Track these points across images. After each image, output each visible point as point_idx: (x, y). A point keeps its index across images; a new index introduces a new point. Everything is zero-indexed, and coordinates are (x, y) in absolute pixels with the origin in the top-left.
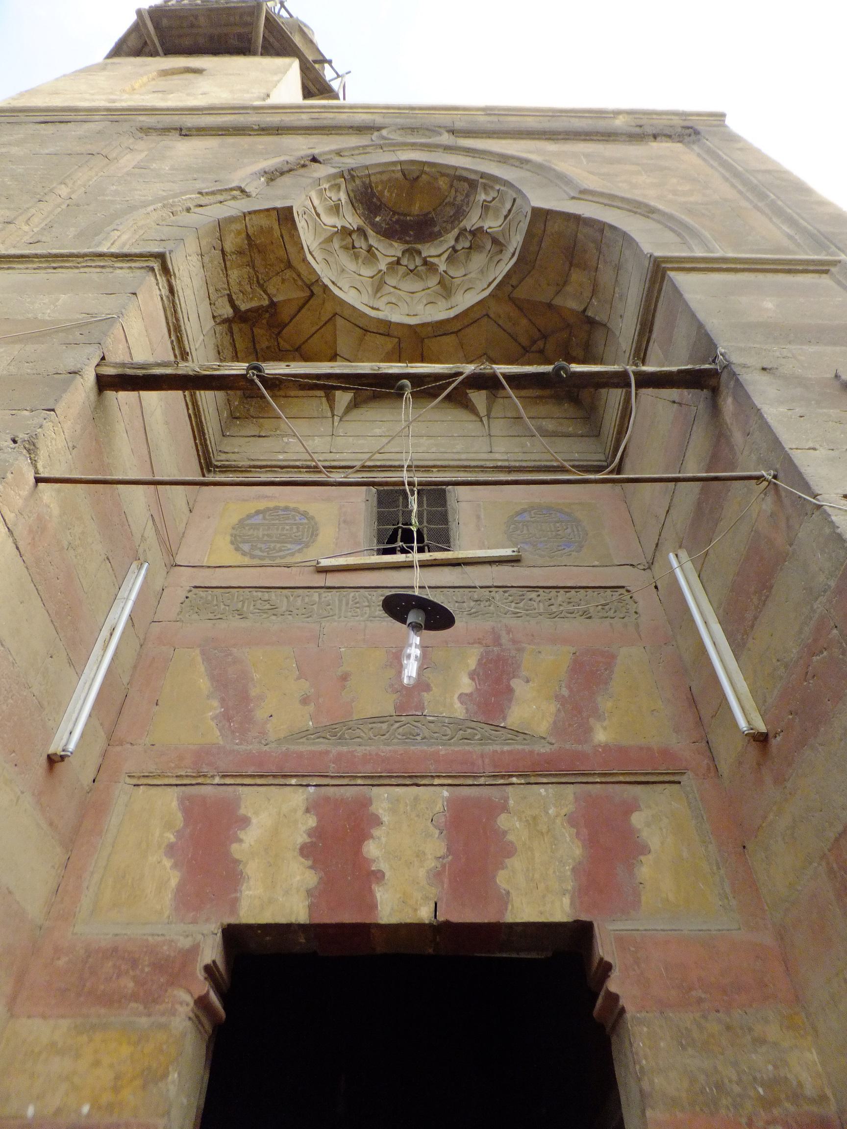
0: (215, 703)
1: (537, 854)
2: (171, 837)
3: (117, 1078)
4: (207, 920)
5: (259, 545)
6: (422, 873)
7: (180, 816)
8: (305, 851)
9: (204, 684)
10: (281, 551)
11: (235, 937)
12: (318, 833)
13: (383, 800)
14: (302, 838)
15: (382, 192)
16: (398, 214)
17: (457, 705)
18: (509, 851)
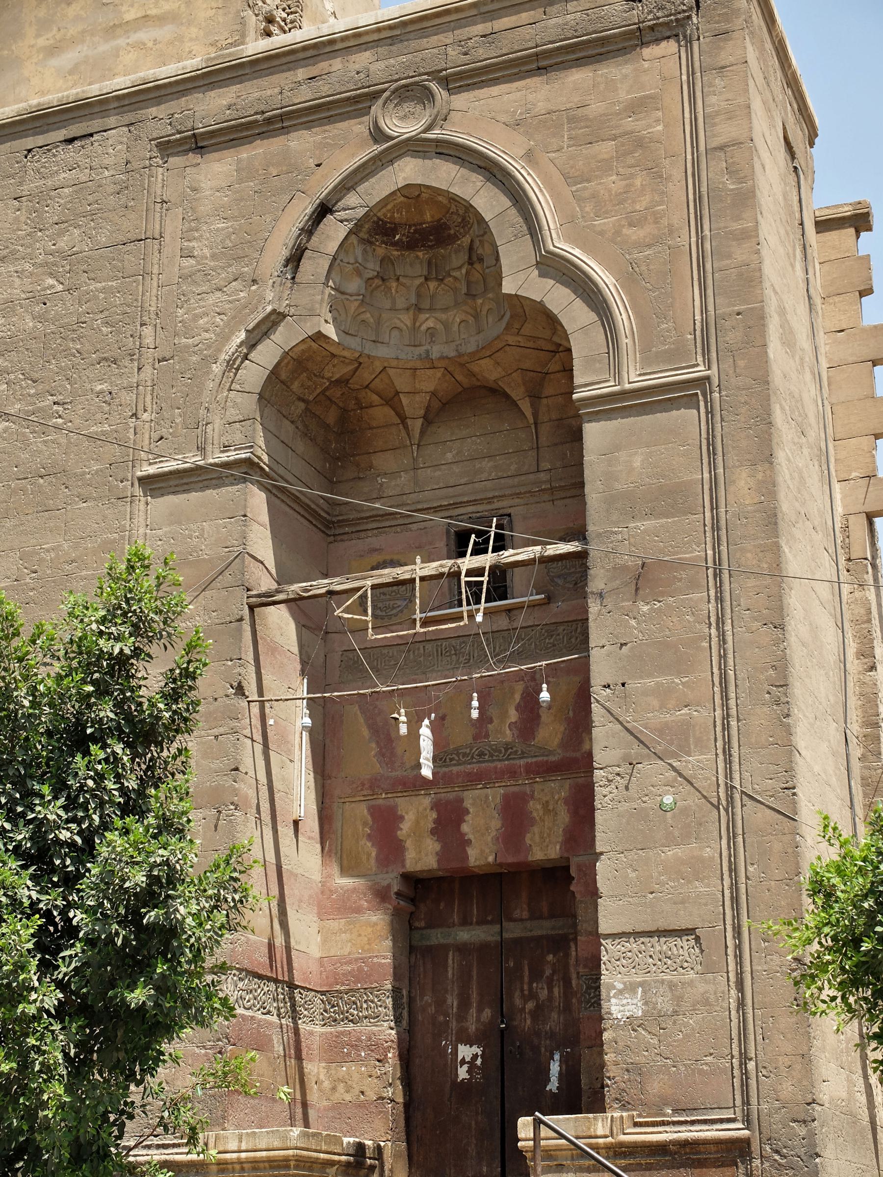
0: (374, 745)
1: (546, 823)
3: (369, 940)
6: (489, 839)
7: (369, 817)
8: (433, 832)
9: (366, 733)
10: (394, 608)
12: (437, 821)
14: (431, 825)
15: (392, 217)
16: (414, 225)
17: (508, 732)
18: (533, 822)
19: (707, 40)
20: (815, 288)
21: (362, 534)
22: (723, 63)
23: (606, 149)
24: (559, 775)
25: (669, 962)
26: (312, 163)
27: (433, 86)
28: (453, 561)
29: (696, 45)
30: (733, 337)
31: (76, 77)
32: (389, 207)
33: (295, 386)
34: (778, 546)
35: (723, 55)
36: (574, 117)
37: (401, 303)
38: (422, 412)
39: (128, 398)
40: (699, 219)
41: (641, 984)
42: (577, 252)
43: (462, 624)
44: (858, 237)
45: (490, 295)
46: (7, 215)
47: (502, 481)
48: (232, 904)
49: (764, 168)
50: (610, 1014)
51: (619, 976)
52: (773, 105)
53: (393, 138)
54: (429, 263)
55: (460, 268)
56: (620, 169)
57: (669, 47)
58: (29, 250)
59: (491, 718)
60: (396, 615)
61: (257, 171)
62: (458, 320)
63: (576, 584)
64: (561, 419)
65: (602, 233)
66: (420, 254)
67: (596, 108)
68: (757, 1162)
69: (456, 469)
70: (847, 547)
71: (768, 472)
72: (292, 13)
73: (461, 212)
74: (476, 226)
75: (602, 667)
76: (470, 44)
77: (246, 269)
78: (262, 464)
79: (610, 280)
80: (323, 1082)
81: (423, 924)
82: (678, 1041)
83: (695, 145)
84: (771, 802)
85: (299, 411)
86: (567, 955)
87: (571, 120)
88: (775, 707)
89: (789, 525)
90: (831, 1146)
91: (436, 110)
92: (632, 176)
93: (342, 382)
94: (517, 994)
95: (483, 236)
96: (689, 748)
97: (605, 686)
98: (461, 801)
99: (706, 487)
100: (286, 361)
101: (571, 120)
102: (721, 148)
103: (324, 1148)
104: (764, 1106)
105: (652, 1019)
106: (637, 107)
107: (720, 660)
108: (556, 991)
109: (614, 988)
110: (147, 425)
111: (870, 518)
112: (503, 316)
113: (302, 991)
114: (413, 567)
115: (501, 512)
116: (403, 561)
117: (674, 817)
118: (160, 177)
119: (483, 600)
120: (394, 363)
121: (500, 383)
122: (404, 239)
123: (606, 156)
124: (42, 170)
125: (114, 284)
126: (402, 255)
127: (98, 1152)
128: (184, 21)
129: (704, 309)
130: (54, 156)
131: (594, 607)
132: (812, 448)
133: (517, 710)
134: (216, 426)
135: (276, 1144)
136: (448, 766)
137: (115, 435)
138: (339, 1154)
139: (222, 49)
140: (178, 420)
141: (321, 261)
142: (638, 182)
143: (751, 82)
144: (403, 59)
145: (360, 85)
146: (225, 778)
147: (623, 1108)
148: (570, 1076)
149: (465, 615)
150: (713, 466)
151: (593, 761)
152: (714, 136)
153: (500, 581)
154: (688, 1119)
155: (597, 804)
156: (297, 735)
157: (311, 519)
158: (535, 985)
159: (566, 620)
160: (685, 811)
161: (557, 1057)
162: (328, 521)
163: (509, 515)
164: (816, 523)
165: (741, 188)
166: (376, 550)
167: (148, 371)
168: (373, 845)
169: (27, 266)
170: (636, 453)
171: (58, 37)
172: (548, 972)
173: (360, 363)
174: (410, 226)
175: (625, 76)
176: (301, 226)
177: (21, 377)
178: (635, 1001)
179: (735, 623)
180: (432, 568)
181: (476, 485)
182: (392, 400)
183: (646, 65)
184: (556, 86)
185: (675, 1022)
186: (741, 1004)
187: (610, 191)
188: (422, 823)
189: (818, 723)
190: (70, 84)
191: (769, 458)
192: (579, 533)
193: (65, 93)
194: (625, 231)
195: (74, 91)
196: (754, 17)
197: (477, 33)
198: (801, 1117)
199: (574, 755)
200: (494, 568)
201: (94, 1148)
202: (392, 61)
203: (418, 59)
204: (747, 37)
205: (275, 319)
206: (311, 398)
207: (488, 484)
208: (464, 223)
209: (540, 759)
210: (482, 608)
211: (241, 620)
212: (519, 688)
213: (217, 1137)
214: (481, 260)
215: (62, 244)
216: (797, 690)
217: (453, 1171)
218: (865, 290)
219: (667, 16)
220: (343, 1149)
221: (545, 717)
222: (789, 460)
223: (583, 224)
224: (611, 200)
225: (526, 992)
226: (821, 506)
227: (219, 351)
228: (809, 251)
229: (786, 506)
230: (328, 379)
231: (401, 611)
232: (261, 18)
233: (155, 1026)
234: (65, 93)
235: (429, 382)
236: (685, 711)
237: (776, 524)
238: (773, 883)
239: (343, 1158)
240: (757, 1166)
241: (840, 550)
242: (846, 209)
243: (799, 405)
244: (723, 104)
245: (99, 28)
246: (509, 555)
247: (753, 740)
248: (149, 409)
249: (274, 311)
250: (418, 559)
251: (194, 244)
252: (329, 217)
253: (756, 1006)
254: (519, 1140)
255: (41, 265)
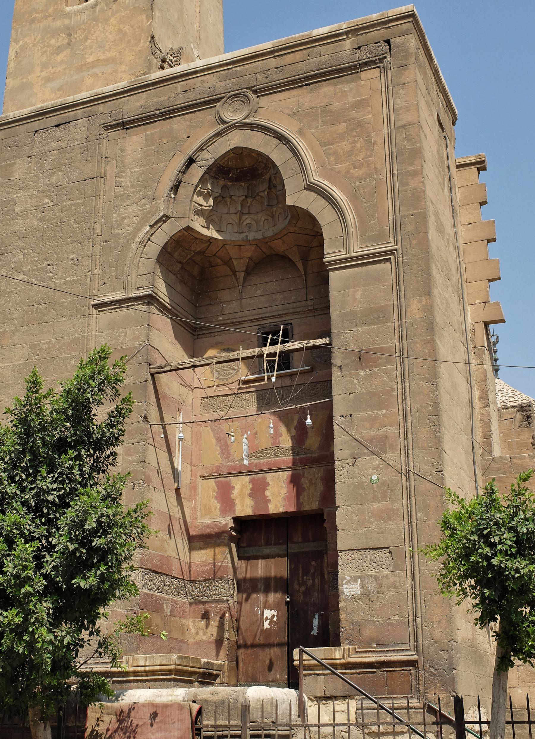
0: (218, 448)
2: (215, 494)
4: (228, 516)
5: (222, 373)
6: (280, 499)
7: (216, 487)
8: (250, 495)
9: (214, 441)
10: (229, 375)
11: (236, 520)
12: (252, 489)
13: (270, 477)
14: (249, 491)
19: (395, 69)
20: (456, 201)
21: (212, 335)
22: (404, 82)
23: (341, 127)
24: (317, 464)
25: (375, 565)
26: (185, 136)
27: (250, 94)
28: (259, 349)
29: (389, 72)
30: (410, 228)
31: (61, 92)
32: (226, 159)
33: (176, 255)
34: (434, 341)
35: (403, 77)
36: (325, 111)
37: (232, 210)
38: (244, 269)
39: (86, 262)
40: (391, 164)
41: (360, 577)
42: (326, 182)
43: (264, 383)
44: (479, 174)
45: (280, 206)
46: (24, 165)
47: (287, 305)
48: (137, 534)
49: (426, 137)
50: (343, 593)
51: (348, 572)
52: (431, 103)
53: (227, 123)
54: (248, 188)
55: (264, 191)
56: (349, 138)
57: (374, 73)
58: (36, 184)
59: (282, 434)
60: (230, 378)
61: (156, 140)
62: (263, 219)
63: (326, 361)
64: (319, 272)
65: (339, 172)
66: (243, 184)
67: (336, 105)
68: (422, 673)
69: (262, 299)
70: (474, 341)
71: (428, 301)
72: (175, 57)
73: (264, 161)
74: (272, 169)
75: (340, 404)
76: (269, 72)
77: (150, 193)
78: (157, 297)
79: (344, 197)
80: (191, 629)
81: (245, 545)
82: (380, 607)
83: (389, 125)
84: (429, 478)
85: (178, 268)
86: (322, 561)
87: (323, 112)
88: (432, 427)
89: (440, 329)
90: (462, 664)
91: (251, 108)
92: (356, 142)
93: (202, 253)
94: (296, 583)
95: (276, 174)
96: (386, 449)
97: (341, 416)
98: (265, 478)
99: (396, 308)
100: (171, 242)
101: (324, 112)
102: (403, 126)
103: (191, 665)
104: (426, 643)
105: (366, 595)
106: (358, 105)
107: (403, 402)
108: (316, 580)
109: (345, 579)
110: (97, 277)
111: (486, 324)
112: (287, 217)
113: (180, 580)
114: (238, 352)
115: (287, 322)
116: (234, 348)
117: (378, 486)
118: (105, 144)
119: (276, 370)
120: (229, 243)
121: (286, 253)
122: (234, 176)
123: (341, 131)
124: (43, 141)
125: (80, 201)
126: (233, 185)
127: (64, 665)
128: (118, 62)
129: (394, 213)
130: (49, 134)
131: (335, 374)
132: (454, 287)
133: (295, 429)
134: (134, 277)
135: (165, 662)
136: (258, 460)
137: (80, 282)
138: (199, 668)
139: (138, 76)
140: (113, 274)
141: (189, 188)
142: (358, 145)
143: (419, 92)
144: (234, 80)
145: (210, 95)
146: (138, 466)
147: (350, 644)
148: (324, 627)
149: (266, 378)
150: (399, 298)
151: (334, 457)
152: (399, 120)
153: (286, 359)
154: (385, 650)
155: (337, 480)
156: (177, 443)
157: (185, 326)
158: (305, 578)
159: (321, 380)
160: (383, 484)
161: (317, 616)
162: (194, 327)
163: (291, 324)
164: (456, 328)
165: (414, 148)
166: (220, 343)
167: (97, 248)
168: (218, 502)
169: (35, 193)
170: (358, 290)
171: (52, 72)
172: (312, 571)
173: (211, 243)
174: (237, 169)
175: (351, 89)
176: (179, 170)
177: (31, 251)
178: (356, 586)
179: (411, 382)
180: (248, 353)
181: (274, 308)
182: (228, 262)
183: (363, 83)
184: (315, 94)
185: (378, 598)
186: (413, 587)
187: (343, 150)
188: (244, 490)
189: (456, 436)
190: (58, 96)
191: (429, 293)
192: (327, 333)
193: (55, 101)
194: (351, 171)
195: (60, 100)
196: (421, 57)
197: (272, 67)
198: (446, 648)
199: (326, 453)
200: (281, 353)
201: (62, 664)
202: (227, 82)
203: (241, 81)
204: (416, 68)
205: (165, 218)
206: (184, 261)
207: (280, 307)
208: (266, 167)
209: (308, 455)
210: (275, 374)
211: (146, 381)
212: (296, 417)
213: (133, 658)
214: (275, 187)
215: (53, 181)
216: (445, 418)
217: (261, 677)
218: (483, 202)
219: (374, 57)
220: (201, 665)
221: (310, 433)
222: (440, 294)
223: (329, 167)
224: (344, 155)
225: (300, 582)
226: (459, 319)
227: (135, 236)
228: (452, 181)
229: (439, 319)
230: (194, 251)
231: (233, 376)
232: (159, 60)
233: (98, 598)
234: (55, 101)
235: (248, 252)
236: (384, 429)
237: (433, 328)
238: (431, 523)
239: (201, 670)
240: (422, 675)
241: (469, 342)
242: (473, 158)
243: (446, 264)
244: (404, 104)
245: (74, 66)
246: (289, 346)
247: (420, 445)
248: (98, 268)
249: (164, 215)
250: (241, 348)
251: (122, 179)
252: (194, 164)
253: (421, 589)
254: (294, 661)
255: (42, 192)
